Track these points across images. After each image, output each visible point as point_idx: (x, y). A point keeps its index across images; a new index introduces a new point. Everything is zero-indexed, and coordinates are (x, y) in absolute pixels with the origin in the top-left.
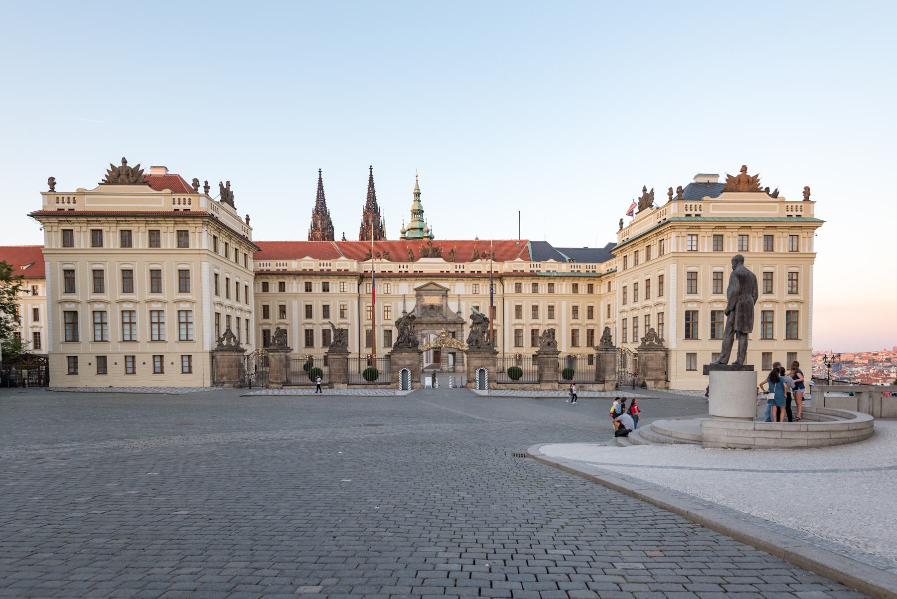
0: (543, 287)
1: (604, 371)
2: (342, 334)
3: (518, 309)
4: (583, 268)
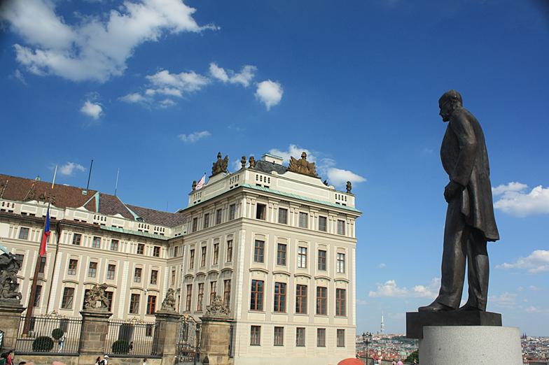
0: (149, 249)
1: (163, 342)
2: (108, 296)
3: (260, 245)
4: (152, 230)
